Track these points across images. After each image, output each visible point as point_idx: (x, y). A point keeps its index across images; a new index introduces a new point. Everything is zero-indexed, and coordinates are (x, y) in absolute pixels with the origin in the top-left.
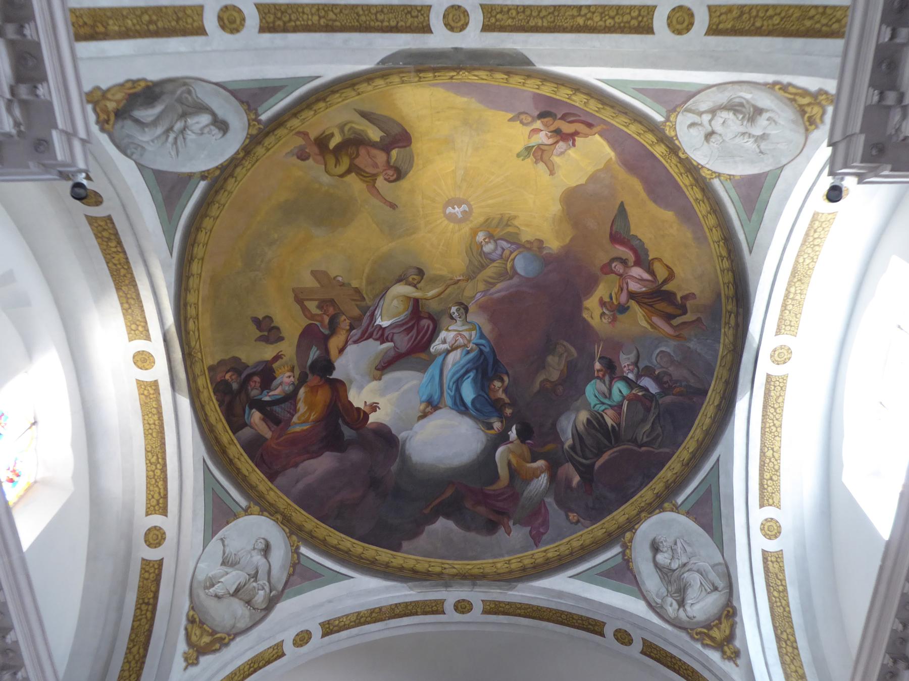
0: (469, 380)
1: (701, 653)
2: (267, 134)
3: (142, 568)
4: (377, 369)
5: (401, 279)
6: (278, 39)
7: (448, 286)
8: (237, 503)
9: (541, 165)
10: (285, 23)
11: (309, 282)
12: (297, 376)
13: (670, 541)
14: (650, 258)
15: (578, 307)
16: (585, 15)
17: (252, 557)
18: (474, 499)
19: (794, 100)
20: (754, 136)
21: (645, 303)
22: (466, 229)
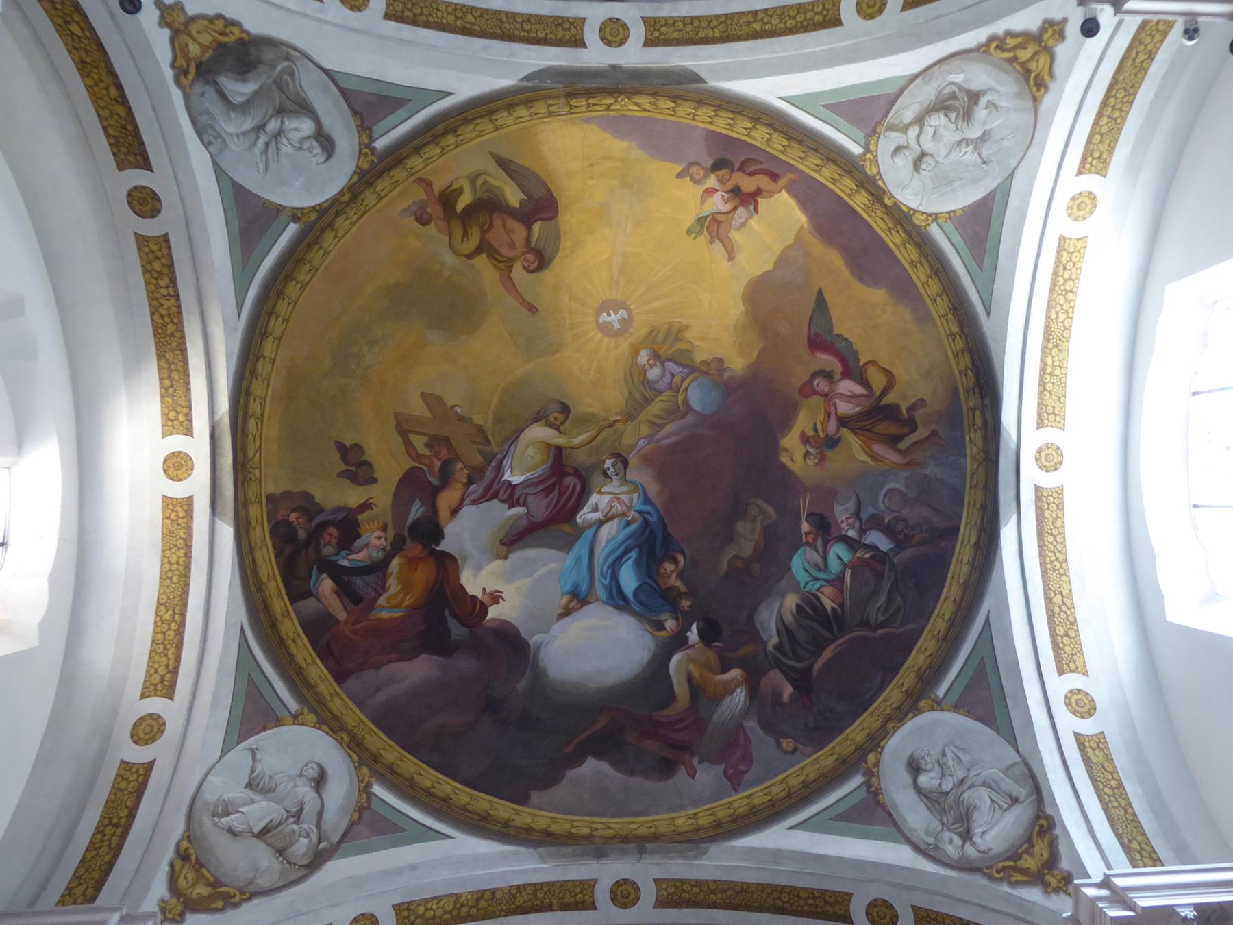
0: (630, 562)
1: (1009, 898)
2: (380, 174)
3: (118, 775)
4: (502, 543)
5: (539, 417)
6: (406, 31)
7: (602, 429)
8: (285, 705)
9: (717, 245)
10: (415, 15)
11: (418, 408)
12: (390, 538)
13: (936, 752)
14: (861, 363)
15: (773, 449)
16: (762, 20)
17: (295, 786)
18: (640, 729)
19: (1015, 58)
20: (972, 140)
21: (861, 428)
22: (625, 345)
